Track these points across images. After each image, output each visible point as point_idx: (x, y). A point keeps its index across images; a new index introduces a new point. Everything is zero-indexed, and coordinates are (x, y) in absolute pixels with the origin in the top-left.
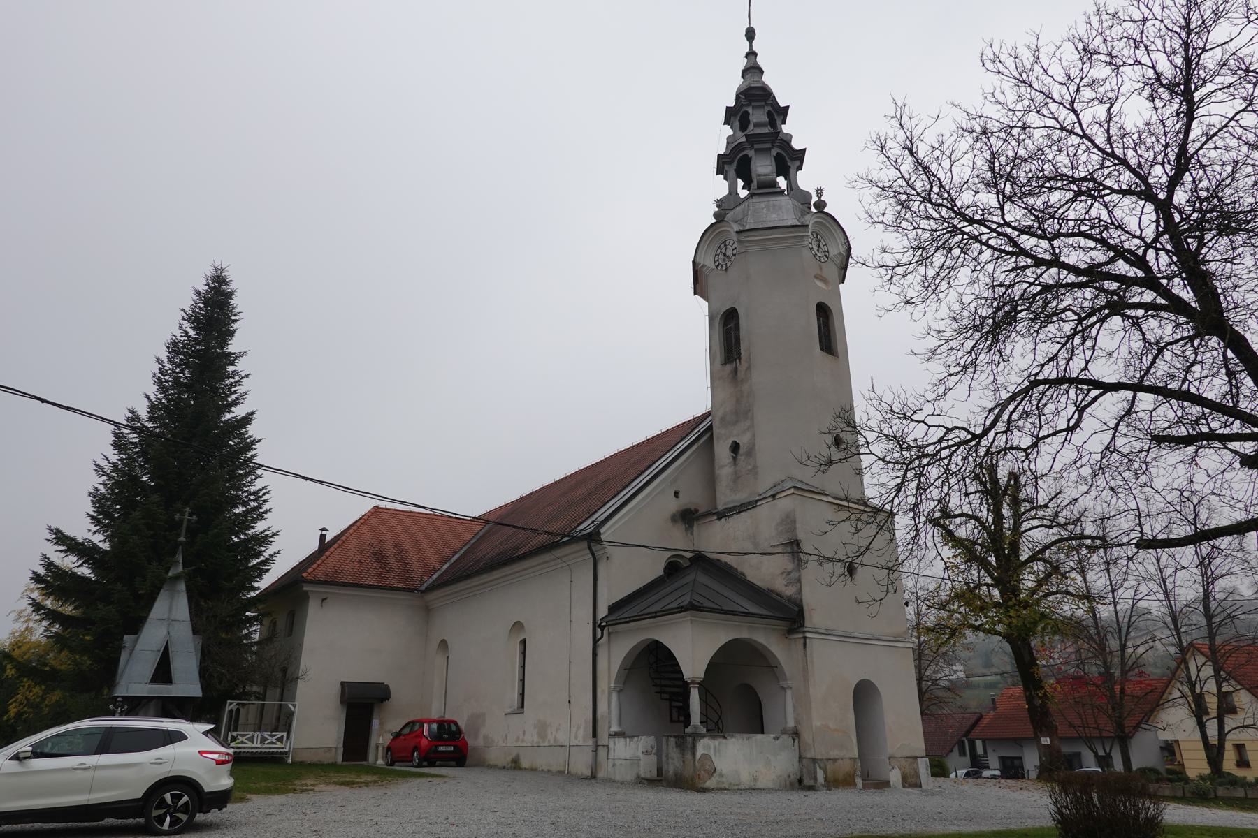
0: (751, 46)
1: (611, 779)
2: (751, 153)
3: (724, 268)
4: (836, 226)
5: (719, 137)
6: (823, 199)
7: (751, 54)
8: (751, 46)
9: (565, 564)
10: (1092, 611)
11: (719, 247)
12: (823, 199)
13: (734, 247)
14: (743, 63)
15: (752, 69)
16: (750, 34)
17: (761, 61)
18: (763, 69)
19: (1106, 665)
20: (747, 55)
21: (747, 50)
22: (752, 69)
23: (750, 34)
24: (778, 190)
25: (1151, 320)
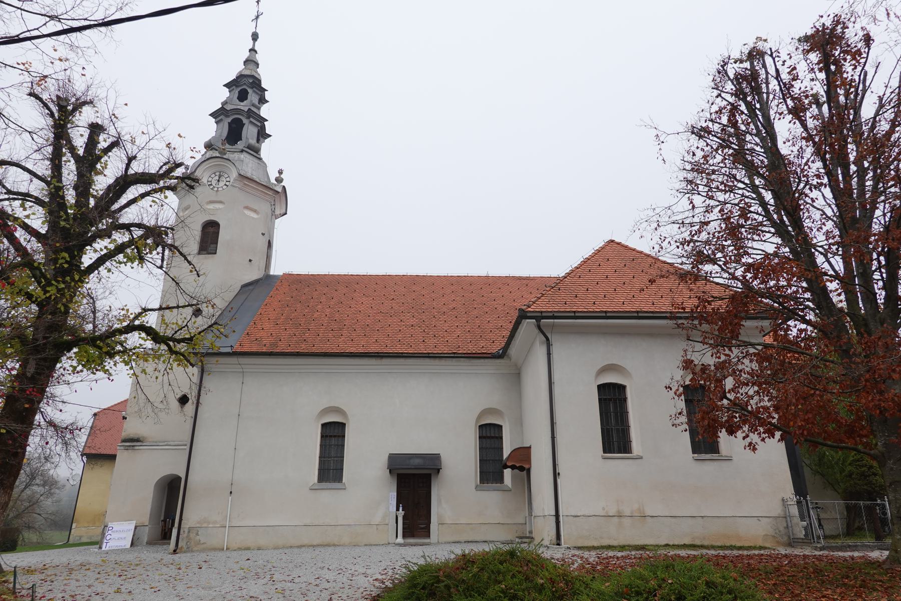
0: (254, 45)
1: (610, 546)
2: (245, 121)
3: (216, 189)
4: (284, 198)
5: (220, 96)
6: (282, 176)
7: (253, 50)
8: (254, 45)
9: (241, 370)
10: (875, 271)
11: (214, 173)
12: (282, 176)
13: (227, 183)
14: (246, 54)
15: (251, 62)
16: (255, 37)
17: (259, 58)
18: (259, 62)
19: (833, 220)
20: (250, 50)
21: (251, 47)
22: (251, 62)
23: (255, 37)
24: (258, 156)
25: (169, 193)
